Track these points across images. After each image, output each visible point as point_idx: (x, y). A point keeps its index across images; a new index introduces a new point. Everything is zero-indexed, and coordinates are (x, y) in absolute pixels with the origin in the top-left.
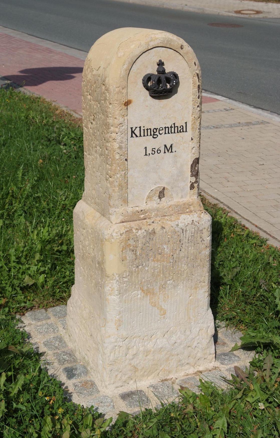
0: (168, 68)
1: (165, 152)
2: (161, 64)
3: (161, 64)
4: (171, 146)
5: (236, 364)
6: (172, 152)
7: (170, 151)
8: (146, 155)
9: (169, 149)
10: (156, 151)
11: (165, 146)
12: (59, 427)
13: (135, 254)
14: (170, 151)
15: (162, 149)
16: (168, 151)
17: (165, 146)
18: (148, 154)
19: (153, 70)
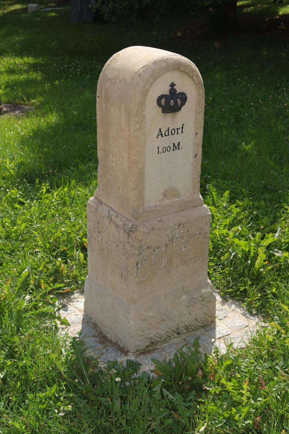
0: (179, 89)
1: (174, 150)
2: (172, 85)
3: (172, 85)
4: (179, 143)
5: (129, 358)
6: (179, 149)
7: (178, 148)
8: (159, 153)
9: (177, 147)
10: (166, 149)
11: (174, 144)
12: (151, 349)
13: (158, 342)
14: (178, 148)
15: (172, 146)
16: (176, 148)
17: (174, 144)
18: (160, 152)
19: (166, 91)
